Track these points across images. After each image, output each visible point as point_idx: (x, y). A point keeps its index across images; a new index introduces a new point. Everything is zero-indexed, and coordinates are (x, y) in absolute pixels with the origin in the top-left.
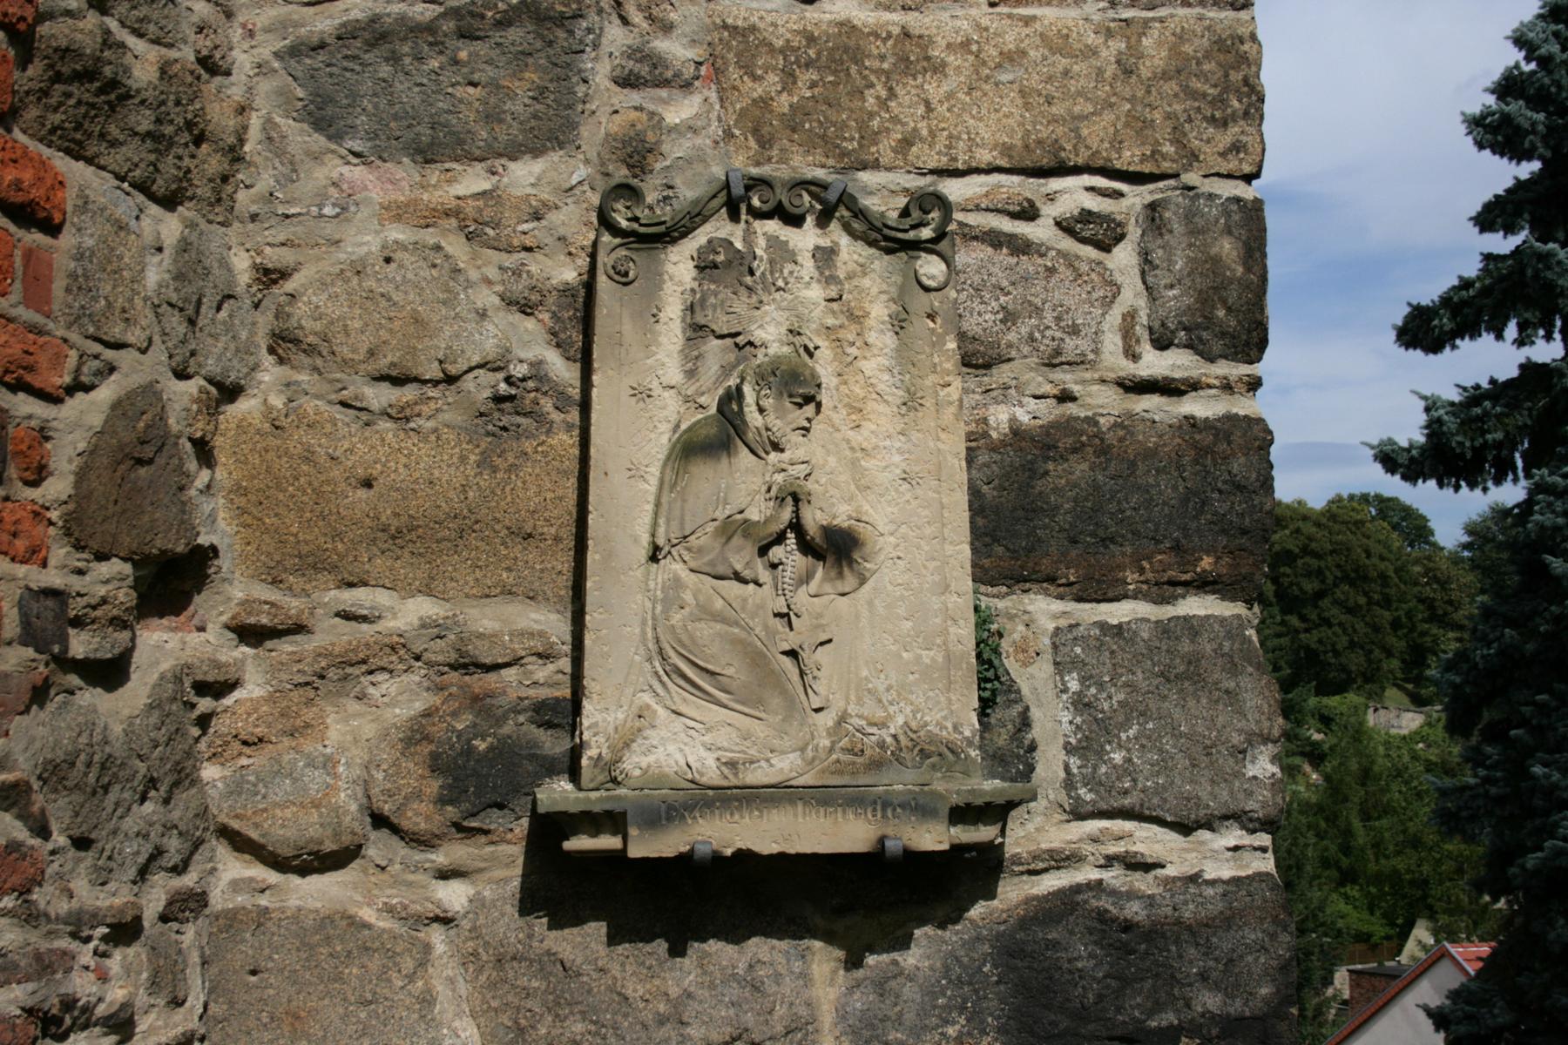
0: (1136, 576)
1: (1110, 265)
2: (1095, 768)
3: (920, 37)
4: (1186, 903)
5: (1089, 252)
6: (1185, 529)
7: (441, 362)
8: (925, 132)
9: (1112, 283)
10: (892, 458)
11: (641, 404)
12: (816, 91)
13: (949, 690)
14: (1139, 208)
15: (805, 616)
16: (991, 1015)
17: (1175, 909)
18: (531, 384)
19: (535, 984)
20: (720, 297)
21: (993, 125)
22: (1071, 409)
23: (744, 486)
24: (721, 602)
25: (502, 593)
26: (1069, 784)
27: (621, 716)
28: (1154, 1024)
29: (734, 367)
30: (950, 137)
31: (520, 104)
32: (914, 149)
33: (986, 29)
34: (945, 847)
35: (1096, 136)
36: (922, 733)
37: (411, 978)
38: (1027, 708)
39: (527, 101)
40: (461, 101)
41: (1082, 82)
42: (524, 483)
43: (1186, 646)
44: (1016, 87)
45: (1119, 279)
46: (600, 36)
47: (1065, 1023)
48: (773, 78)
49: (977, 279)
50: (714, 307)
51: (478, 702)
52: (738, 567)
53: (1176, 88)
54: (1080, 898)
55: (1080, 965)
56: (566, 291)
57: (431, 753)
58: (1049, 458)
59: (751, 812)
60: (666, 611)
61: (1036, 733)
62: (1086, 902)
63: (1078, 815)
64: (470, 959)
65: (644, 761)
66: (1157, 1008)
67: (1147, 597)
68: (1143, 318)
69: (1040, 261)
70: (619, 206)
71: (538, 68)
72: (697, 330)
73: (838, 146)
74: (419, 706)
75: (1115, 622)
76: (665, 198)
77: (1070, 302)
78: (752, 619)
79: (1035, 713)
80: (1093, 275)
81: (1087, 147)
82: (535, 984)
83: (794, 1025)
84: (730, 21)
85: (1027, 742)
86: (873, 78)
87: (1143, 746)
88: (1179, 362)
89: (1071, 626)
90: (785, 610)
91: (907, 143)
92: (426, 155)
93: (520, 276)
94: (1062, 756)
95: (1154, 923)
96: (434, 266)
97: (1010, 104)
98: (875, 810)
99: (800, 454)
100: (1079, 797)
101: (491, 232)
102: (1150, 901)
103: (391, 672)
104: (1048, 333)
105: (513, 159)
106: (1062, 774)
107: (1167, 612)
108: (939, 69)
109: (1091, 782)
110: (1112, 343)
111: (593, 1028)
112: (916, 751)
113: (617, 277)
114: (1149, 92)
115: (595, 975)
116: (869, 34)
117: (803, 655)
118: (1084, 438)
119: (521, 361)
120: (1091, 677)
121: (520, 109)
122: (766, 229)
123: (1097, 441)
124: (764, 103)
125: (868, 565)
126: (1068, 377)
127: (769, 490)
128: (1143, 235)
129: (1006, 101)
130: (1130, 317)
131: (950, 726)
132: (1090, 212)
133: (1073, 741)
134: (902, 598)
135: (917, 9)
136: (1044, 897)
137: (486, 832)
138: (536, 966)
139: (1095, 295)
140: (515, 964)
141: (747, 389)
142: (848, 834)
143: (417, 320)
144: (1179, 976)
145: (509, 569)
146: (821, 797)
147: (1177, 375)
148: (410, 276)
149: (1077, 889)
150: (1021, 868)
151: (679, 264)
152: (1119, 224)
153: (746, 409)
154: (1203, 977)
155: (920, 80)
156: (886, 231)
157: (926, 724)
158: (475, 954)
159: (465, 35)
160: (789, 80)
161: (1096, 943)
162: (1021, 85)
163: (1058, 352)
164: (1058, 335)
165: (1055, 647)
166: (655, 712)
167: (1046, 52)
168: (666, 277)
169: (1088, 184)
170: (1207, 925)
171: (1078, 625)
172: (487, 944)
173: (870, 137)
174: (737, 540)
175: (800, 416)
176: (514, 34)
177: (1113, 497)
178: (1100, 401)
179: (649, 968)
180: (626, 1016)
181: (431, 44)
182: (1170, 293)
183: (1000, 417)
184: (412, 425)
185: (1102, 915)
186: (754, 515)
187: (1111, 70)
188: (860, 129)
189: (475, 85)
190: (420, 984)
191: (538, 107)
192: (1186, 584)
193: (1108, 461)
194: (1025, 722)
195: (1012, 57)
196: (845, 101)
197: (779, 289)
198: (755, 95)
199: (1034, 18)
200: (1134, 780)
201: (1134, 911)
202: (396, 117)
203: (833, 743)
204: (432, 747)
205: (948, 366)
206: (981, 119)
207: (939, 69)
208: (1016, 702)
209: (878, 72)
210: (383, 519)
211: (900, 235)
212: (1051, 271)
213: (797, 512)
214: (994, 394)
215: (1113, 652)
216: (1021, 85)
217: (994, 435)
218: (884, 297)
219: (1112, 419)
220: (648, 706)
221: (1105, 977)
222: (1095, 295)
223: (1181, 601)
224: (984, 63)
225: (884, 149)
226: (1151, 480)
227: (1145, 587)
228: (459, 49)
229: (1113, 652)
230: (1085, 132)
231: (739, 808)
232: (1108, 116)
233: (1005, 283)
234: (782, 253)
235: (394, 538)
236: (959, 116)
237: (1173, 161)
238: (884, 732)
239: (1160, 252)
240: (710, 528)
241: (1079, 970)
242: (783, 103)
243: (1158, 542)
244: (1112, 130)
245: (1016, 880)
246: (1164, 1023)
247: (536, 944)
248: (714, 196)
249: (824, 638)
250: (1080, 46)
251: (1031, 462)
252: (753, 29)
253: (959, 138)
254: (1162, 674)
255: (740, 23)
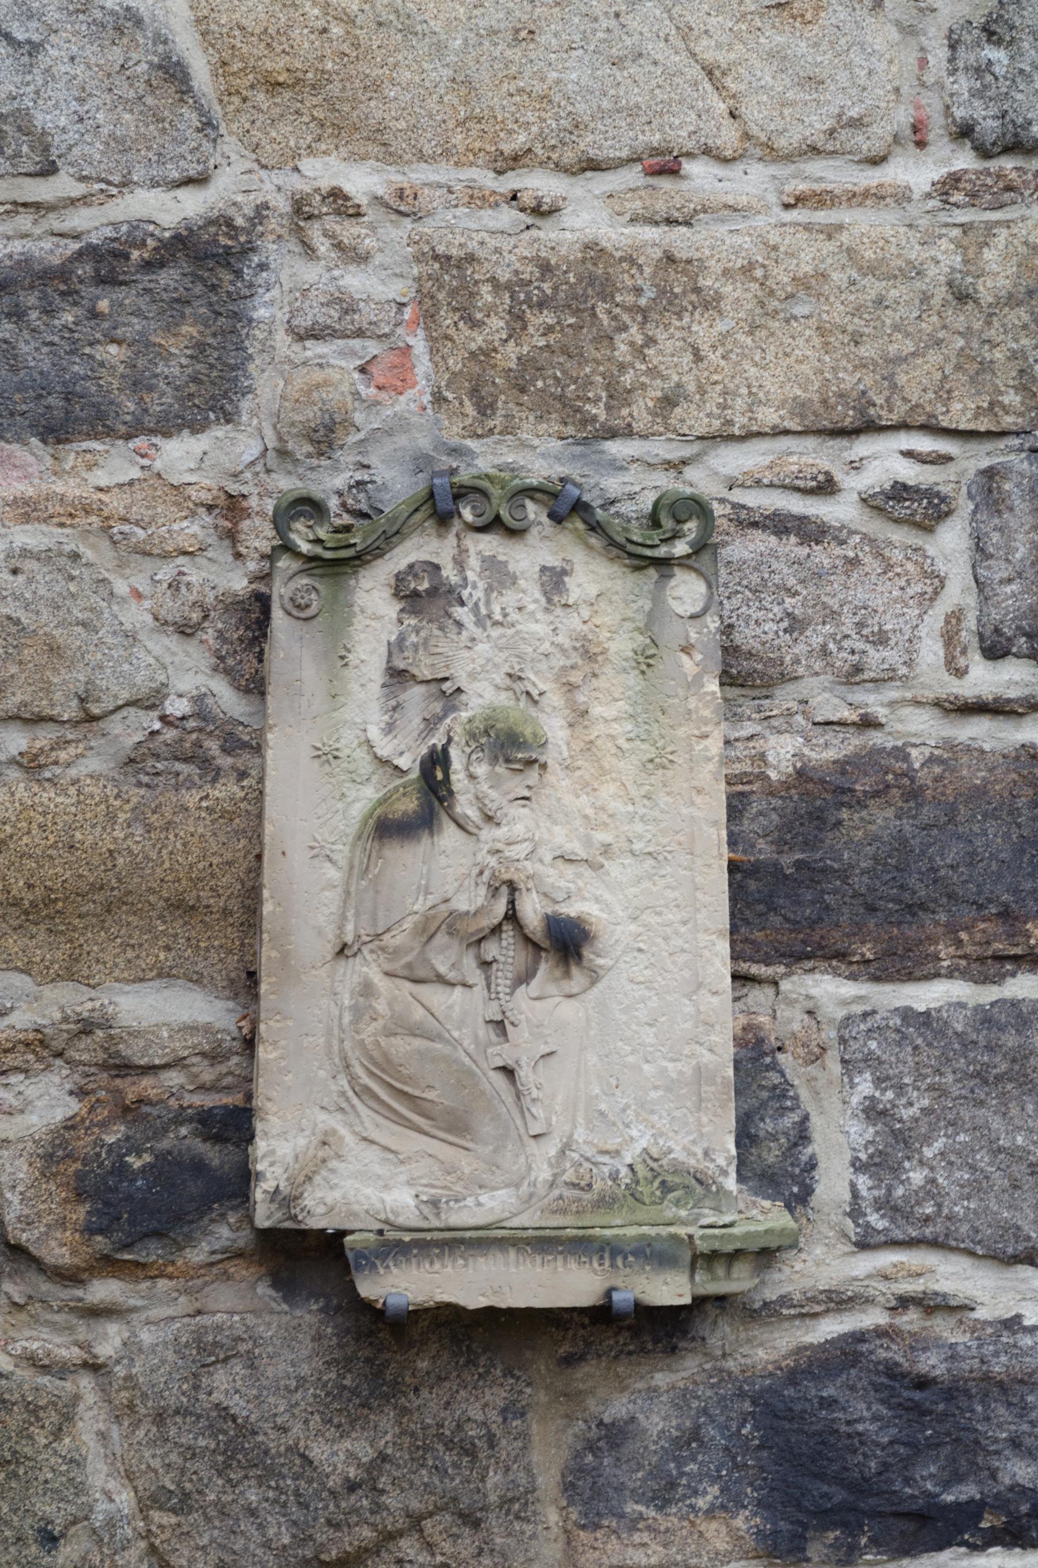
0: (951, 950)
1: (931, 551)
2: (890, 1189)
3: (689, 262)
4: (996, 1354)
5: (899, 535)
6: (1016, 892)
7: (82, 700)
8: (692, 388)
9: (934, 575)
10: (630, 827)
11: (327, 768)
12: (552, 338)
13: (699, 1109)
14: (971, 473)
15: (524, 1026)
16: (751, 1484)
17: (982, 1362)
18: (191, 724)
19: (202, 1442)
20: (423, 634)
21: (782, 373)
22: (876, 738)
23: (445, 869)
24: (421, 1011)
25: (160, 975)
26: (855, 1213)
27: (302, 1142)
28: (950, 1498)
29: (441, 719)
30: (725, 393)
31: (175, 364)
32: (678, 410)
33: (775, 248)
34: (687, 1300)
35: (916, 382)
36: (664, 1162)
37: (57, 1434)
38: (806, 1118)
39: (184, 361)
40: (102, 364)
41: (902, 311)
42: (184, 845)
43: (1010, 1040)
44: (813, 322)
45: (941, 568)
46: (261, 780)
47: (839, 1495)
48: (497, 323)
49: (755, 579)
50: (416, 647)
51: (128, 1111)
52: (442, 969)
53: (1026, 318)
54: (864, 1347)
55: (860, 1428)
56: (233, 605)
57: (77, 1173)
58: (842, 804)
59: (455, 1260)
60: (356, 1021)
61: (816, 1147)
62: (871, 1352)
63: (863, 1245)
64: (125, 1413)
65: (332, 1197)
66: (957, 1478)
67: (965, 975)
68: (971, 622)
69: (838, 551)
70: (299, 525)
71: (198, 320)
72: (398, 676)
73: (578, 410)
74: (59, 1115)
75: (922, 1008)
76: (359, 483)
77: (878, 603)
78: (459, 1029)
79: (816, 1122)
80: (910, 566)
81: (905, 400)
82: (202, 1442)
83: (510, 1495)
84: (441, 249)
85: (804, 1158)
86: (626, 318)
87: (951, 1163)
88: (1017, 677)
89: (865, 1015)
90: (499, 1018)
91: (668, 402)
92: (55, 433)
93: (178, 589)
94: (849, 1173)
95: (955, 1380)
96: (72, 578)
97: (805, 347)
98: (602, 1258)
99: (519, 829)
100: (868, 1225)
101: (141, 534)
102: (953, 1355)
103: (26, 1071)
104: (846, 644)
105: (167, 435)
106: (847, 1196)
107: (989, 994)
108: (711, 303)
109: (885, 1205)
110: (931, 652)
111: (271, 1494)
112: (656, 1184)
113: (295, 612)
114: (989, 323)
115: (273, 1434)
116: (622, 259)
117: (524, 1073)
118: (890, 777)
119: (180, 696)
120: (888, 1078)
121: (176, 371)
122: (481, 547)
123: (906, 781)
124: (488, 352)
125: (600, 961)
126: (871, 698)
127: (481, 873)
128: (974, 512)
129: (800, 341)
130: (955, 617)
131: (699, 1152)
132: (905, 487)
133: (863, 1156)
134: (643, 1000)
135: (688, 224)
136: (820, 1345)
137: (144, 1266)
138: (203, 1423)
139: (910, 592)
140: (178, 1419)
141: (454, 753)
142: (571, 1285)
143: (54, 649)
144: (984, 1442)
145: (168, 948)
146: (543, 1244)
147: (1012, 694)
148: (42, 591)
149: (859, 1337)
150: (792, 1312)
151: (373, 594)
152: (943, 500)
153: (453, 777)
154: (1015, 1443)
155: (687, 319)
156: (630, 548)
157: (670, 1151)
158: (131, 1406)
159: (108, 280)
160: (517, 322)
161: (883, 1402)
162: (820, 320)
163: (857, 669)
164: (860, 645)
165: (843, 1041)
166: (341, 1139)
167: (855, 275)
168: (356, 609)
169: (905, 447)
170: (1022, 1382)
171: (874, 1012)
172: (144, 1396)
173: (618, 396)
174: (441, 939)
175: (517, 786)
176: (167, 278)
177: (923, 852)
178: (913, 728)
179: (338, 1426)
180: (310, 1481)
181: (63, 294)
182: (1008, 589)
183: (783, 753)
184: (48, 774)
185: (891, 1371)
186: (462, 904)
187: (941, 293)
188: (608, 387)
189: (119, 343)
190: (67, 1441)
191: (198, 366)
192: (1015, 959)
193: (919, 806)
194: (802, 1135)
195: (807, 285)
196: (590, 351)
197: (496, 623)
198: (473, 346)
199: (840, 227)
200: (939, 1206)
201: (931, 1363)
202: (21, 387)
203: (555, 1175)
204: (78, 1165)
205: (706, 713)
206: (765, 368)
207: (711, 303)
208: (792, 1109)
209: (634, 309)
210: (14, 892)
211: (648, 552)
212: (853, 563)
213: (512, 902)
214: (775, 723)
215: (916, 1048)
216: (820, 320)
217: (773, 775)
218: (629, 625)
219: (927, 751)
220: (334, 1132)
221: (891, 1443)
222: (910, 592)
223: (1010, 981)
224: (772, 293)
225: (639, 411)
226: (976, 828)
227: (963, 963)
228: (98, 298)
229: (916, 1048)
230: (902, 379)
231: (440, 1256)
232: (934, 357)
233: (791, 582)
234: (500, 577)
235: (27, 913)
236: (738, 363)
237: (1021, 414)
238: (616, 1163)
239: (996, 537)
240: (407, 925)
241: (859, 1434)
242: (510, 354)
243: (980, 907)
244: (939, 375)
245: (786, 1325)
246: (963, 1498)
247: (202, 1397)
248: (416, 510)
249: (545, 1049)
250: (899, 262)
251: (820, 809)
252: (471, 258)
253: (735, 394)
254: (978, 1074)
255: (454, 252)
